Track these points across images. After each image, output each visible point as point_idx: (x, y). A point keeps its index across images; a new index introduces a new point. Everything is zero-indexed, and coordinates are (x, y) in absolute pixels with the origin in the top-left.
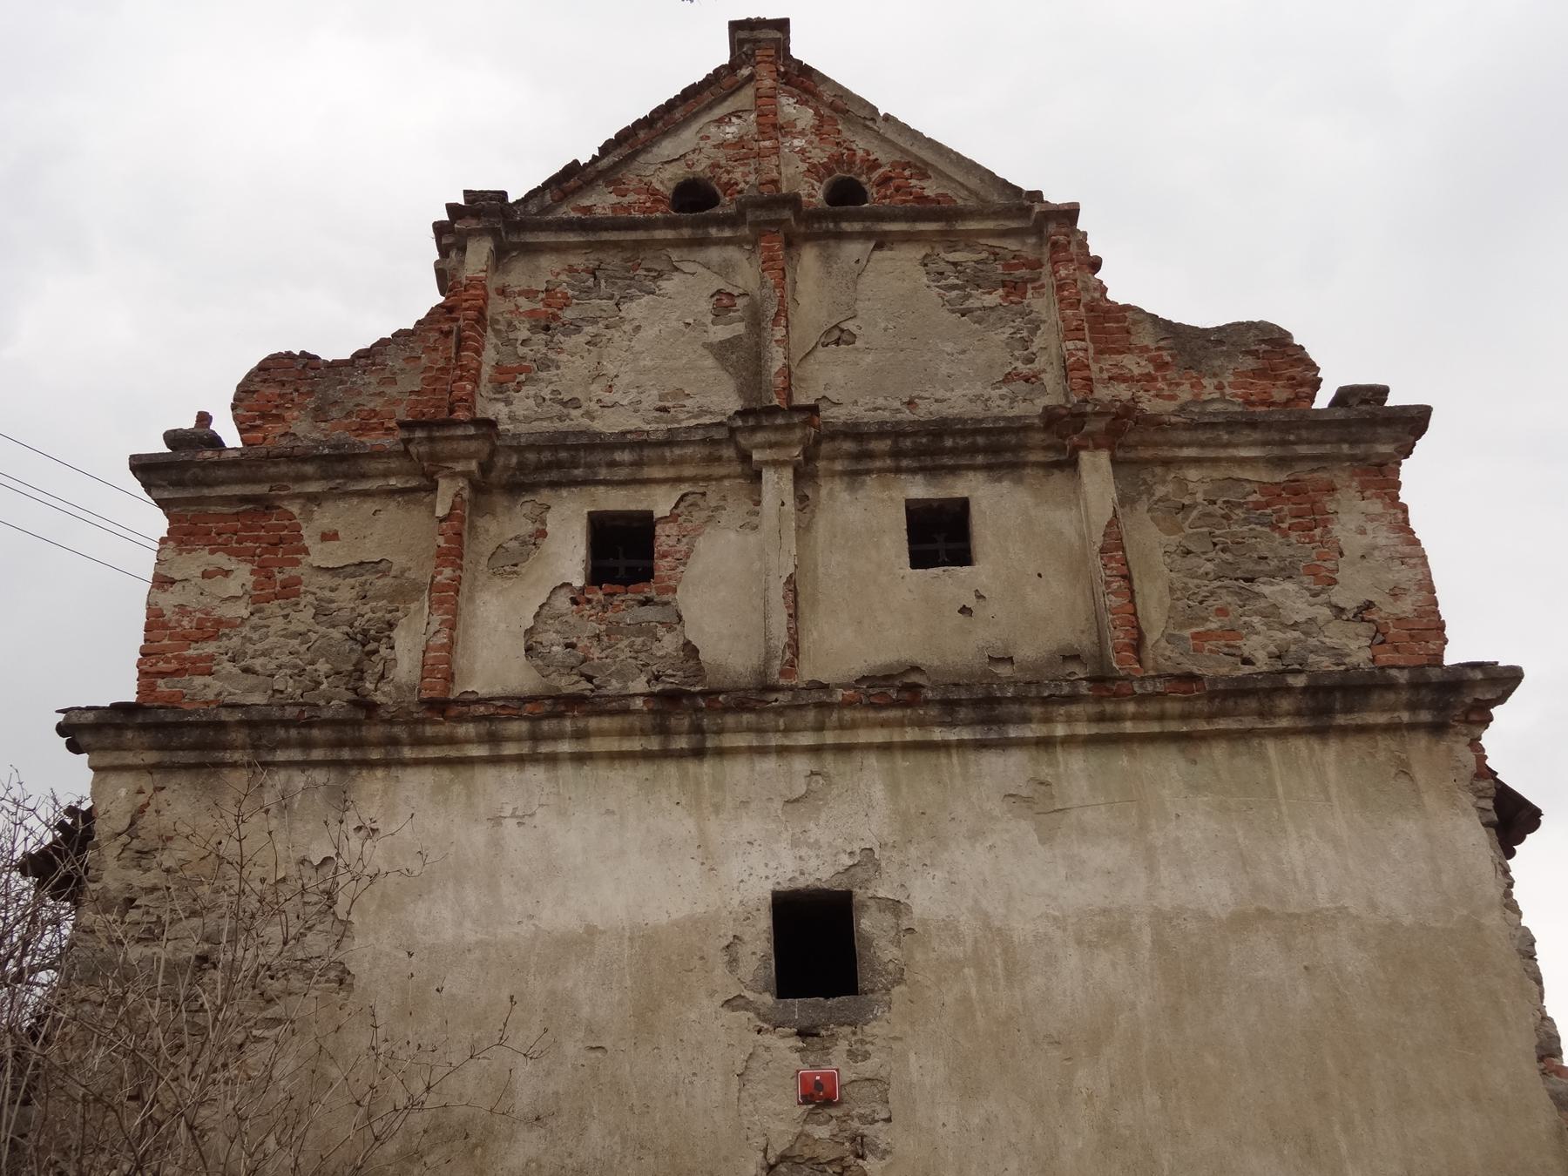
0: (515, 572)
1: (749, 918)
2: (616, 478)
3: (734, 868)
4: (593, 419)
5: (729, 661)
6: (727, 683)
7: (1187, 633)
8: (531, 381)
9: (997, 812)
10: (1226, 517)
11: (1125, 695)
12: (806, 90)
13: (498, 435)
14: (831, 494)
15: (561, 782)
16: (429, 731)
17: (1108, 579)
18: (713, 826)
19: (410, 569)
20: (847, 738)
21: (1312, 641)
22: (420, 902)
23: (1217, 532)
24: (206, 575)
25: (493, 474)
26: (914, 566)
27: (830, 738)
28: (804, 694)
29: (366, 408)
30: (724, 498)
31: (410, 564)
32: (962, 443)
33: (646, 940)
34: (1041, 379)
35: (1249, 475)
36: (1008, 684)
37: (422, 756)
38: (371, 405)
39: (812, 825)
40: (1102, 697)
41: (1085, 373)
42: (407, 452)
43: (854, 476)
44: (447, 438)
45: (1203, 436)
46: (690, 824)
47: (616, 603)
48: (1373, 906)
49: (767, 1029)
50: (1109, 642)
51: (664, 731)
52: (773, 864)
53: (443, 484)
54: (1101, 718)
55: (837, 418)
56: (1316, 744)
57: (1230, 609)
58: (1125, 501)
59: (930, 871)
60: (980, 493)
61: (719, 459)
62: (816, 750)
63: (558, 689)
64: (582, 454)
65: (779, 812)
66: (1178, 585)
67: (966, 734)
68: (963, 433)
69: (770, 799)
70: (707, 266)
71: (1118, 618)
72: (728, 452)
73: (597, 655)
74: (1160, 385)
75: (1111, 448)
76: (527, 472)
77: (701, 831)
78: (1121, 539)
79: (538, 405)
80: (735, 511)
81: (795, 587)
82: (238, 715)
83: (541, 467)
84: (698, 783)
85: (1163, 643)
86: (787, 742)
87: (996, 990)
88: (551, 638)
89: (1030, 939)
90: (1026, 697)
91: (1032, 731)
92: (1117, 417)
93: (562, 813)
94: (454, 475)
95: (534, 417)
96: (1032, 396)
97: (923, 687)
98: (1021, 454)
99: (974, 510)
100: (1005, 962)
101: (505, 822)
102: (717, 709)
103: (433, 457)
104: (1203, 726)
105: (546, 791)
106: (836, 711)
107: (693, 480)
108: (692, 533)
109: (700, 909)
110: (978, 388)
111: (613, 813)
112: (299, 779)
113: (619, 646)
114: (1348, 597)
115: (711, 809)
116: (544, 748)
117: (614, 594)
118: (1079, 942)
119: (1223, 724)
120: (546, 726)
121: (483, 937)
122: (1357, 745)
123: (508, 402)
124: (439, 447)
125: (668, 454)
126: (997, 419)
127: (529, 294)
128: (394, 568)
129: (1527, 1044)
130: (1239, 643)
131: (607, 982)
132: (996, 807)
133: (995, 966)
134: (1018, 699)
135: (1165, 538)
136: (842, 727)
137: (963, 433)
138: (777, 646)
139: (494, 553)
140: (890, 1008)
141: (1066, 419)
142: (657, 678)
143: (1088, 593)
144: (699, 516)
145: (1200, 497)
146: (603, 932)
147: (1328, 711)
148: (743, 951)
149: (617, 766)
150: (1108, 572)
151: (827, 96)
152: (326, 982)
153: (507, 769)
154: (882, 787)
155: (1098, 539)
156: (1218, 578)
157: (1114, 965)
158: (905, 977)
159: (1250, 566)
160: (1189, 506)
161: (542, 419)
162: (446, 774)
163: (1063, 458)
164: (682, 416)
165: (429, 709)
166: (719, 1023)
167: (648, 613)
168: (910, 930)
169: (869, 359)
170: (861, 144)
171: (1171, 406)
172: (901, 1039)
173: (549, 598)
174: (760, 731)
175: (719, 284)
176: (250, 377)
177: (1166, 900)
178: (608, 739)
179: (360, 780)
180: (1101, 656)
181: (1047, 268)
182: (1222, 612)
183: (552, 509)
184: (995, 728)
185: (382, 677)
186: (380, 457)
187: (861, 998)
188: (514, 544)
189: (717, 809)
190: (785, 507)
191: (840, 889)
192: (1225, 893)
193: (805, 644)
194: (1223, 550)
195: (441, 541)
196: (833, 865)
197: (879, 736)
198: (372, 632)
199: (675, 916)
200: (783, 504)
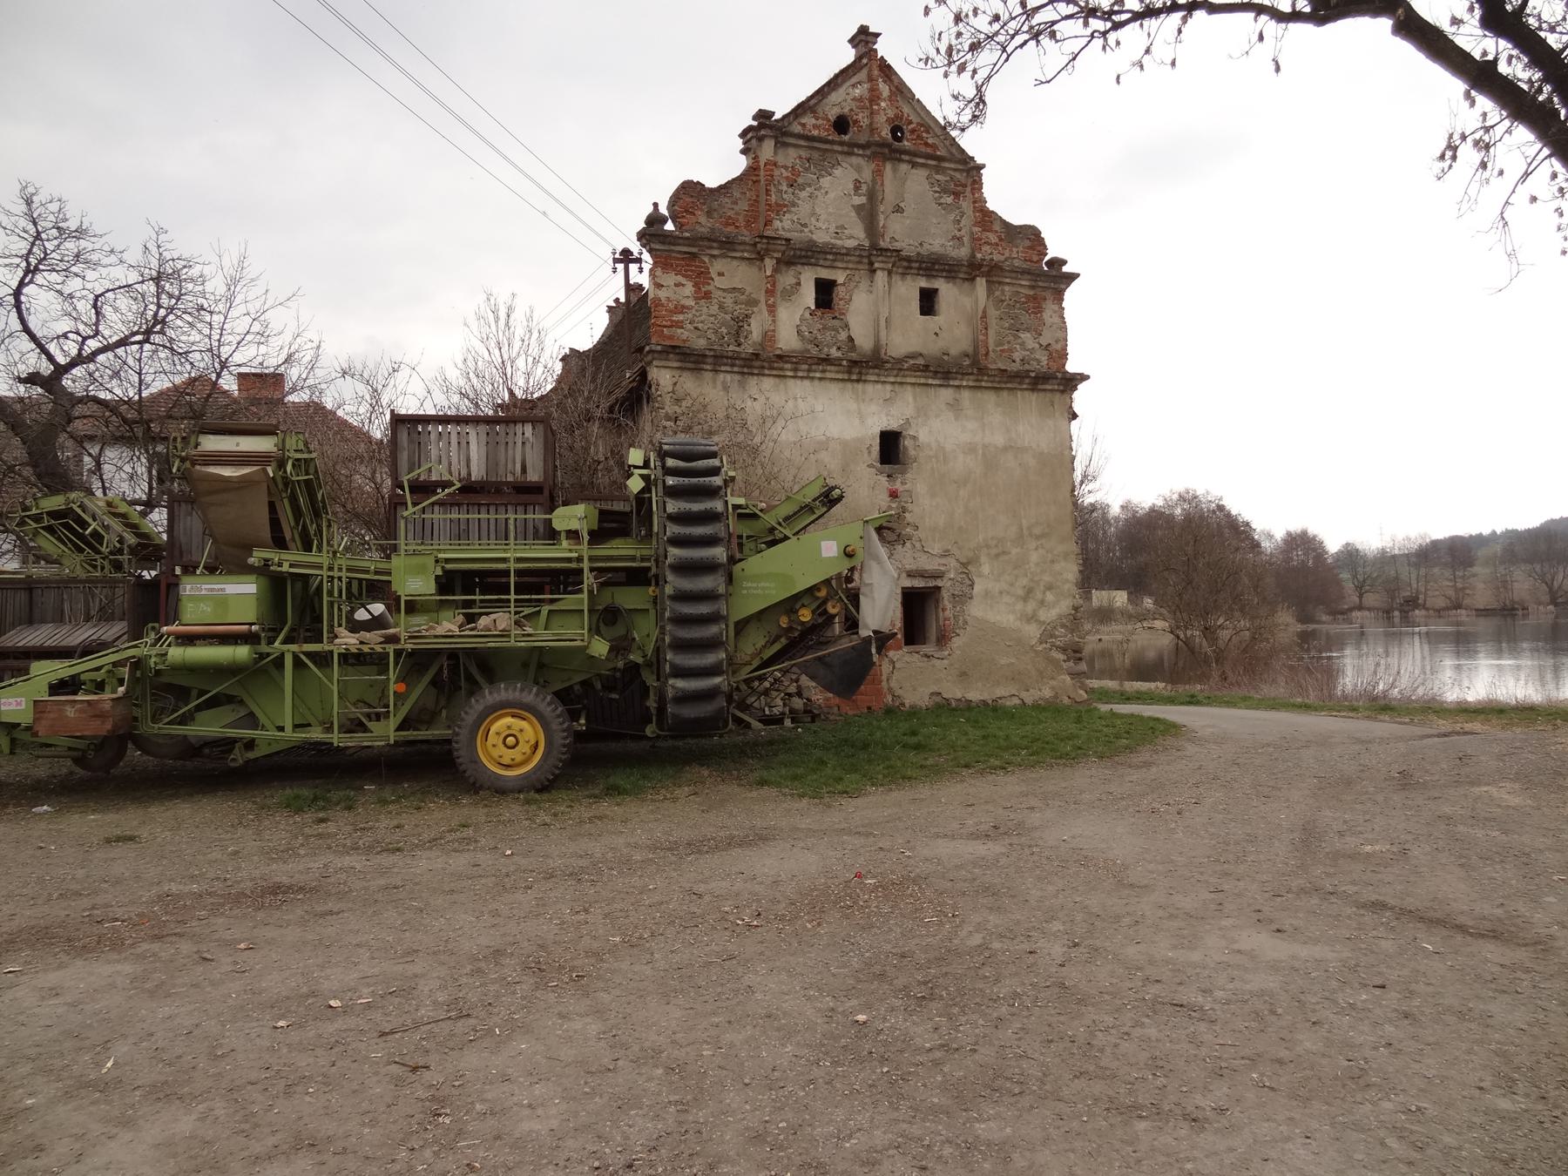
3: (870, 421)
7: (998, 349)
8: (789, 212)
12: (887, 76)
24: (676, 285)
27: (899, 380)
33: (845, 444)
35: (1022, 291)
45: (1014, 275)
48: (1038, 446)
51: (850, 373)
54: (977, 380)
70: (851, 165)
77: (859, 409)
80: (864, 284)
82: (712, 353)
83: (800, 257)
88: (804, 328)
91: (957, 383)
94: (772, 258)
107: (852, 269)
110: (943, 241)
112: (728, 377)
114: (1044, 341)
116: (811, 375)
119: (1009, 385)
120: (814, 367)
122: (1041, 394)
123: (781, 221)
127: (786, 168)
129: (1070, 489)
134: (956, 373)
144: (853, 284)
151: (896, 81)
162: (777, 380)
167: (836, 322)
169: (908, 222)
170: (906, 110)
174: (879, 375)
175: (857, 177)
176: (678, 191)
181: (969, 189)
182: (1009, 342)
197: (913, 380)
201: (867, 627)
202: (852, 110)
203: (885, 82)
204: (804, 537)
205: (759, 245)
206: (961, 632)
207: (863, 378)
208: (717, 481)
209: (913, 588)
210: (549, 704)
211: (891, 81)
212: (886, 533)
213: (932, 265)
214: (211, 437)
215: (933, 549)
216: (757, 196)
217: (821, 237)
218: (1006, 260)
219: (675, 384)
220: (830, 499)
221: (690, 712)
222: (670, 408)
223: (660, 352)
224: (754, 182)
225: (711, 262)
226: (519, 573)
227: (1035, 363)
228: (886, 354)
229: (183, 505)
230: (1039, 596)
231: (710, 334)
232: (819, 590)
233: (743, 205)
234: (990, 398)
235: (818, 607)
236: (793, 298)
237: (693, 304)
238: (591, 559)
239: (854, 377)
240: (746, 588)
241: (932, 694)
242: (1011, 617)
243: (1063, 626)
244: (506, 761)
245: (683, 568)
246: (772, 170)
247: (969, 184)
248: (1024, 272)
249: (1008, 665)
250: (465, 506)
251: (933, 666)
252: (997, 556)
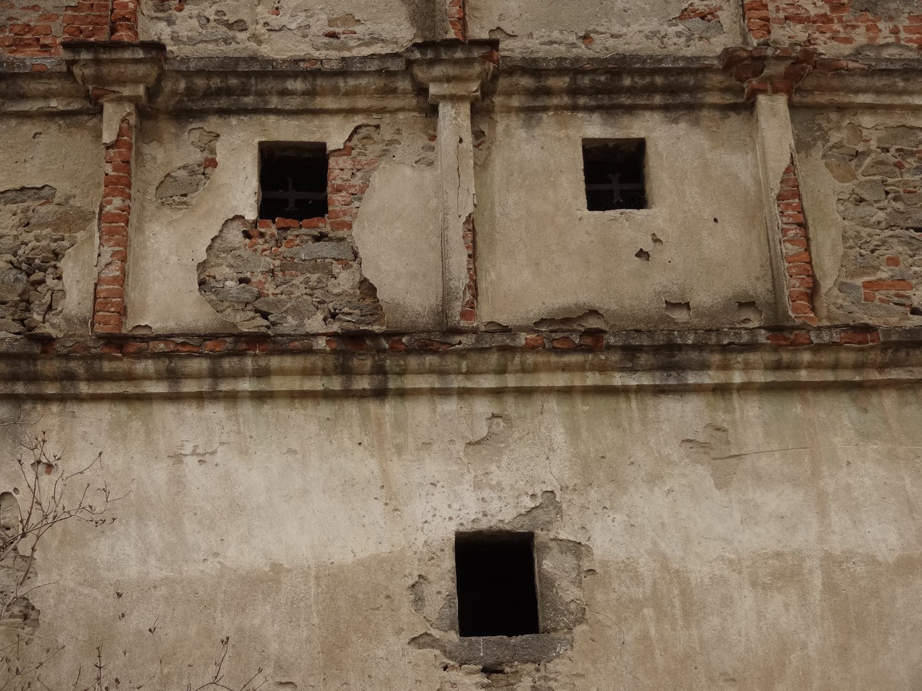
0: (184, 203)
1: (433, 558)
2: (288, 107)
3: (418, 509)
4: (260, 43)
5: (406, 300)
6: (405, 323)
7: (859, 282)
9: (675, 457)
10: (899, 165)
11: (802, 344)
13: (166, 59)
14: (507, 130)
15: (241, 420)
16: (107, 366)
17: (785, 226)
18: (396, 467)
19: (74, 196)
20: (528, 381)
22: (103, 539)
23: (890, 181)
25: (160, 99)
26: (592, 207)
27: (511, 381)
28: (487, 337)
29: (19, 22)
30: (398, 131)
31: (75, 191)
32: (640, 82)
34: (718, 17)
36: (689, 330)
37: (99, 392)
38: (25, 20)
39: (493, 468)
40: (781, 346)
41: (763, 13)
42: (69, 74)
43: (530, 113)
44: (114, 61)
45: (879, 82)
46: (373, 464)
47: (290, 237)
49: (453, 666)
50: (786, 291)
51: (346, 371)
52: (456, 506)
53: (109, 109)
54: (778, 366)
55: (512, 50)
57: (901, 258)
58: (802, 146)
59: (610, 513)
60: (656, 134)
61: (394, 91)
62: (497, 393)
63: (234, 326)
64: (253, 81)
65: (461, 453)
66: (851, 233)
67: (645, 380)
68: (642, 72)
69: (451, 441)
71: (795, 266)
72: (404, 84)
73: (271, 291)
74: (836, 26)
75: (789, 92)
76: (195, 98)
77: (384, 471)
78: (798, 187)
79: (202, 26)
81: (473, 227)
83: (208, 94)
84: (380, 424)
85: (836, 292)
86: (469, 385)
87: (674, 630)
88: (222, 271)
89: (706, 581)
90: (706, 344)
92: (797, 61)
93: (243, 452)
94: (120, 100)
95: (199, 38)
96: (708, 34)
97: (604, 332)
98: (699, 96)
99: (650, 150)
100: (683, 602)
101: (185, 459)
102: (400, 351)
103: (99, 80)
104: (875, 376)
105: (227, 429)
106: (518, 355)
107: (367, 111)
108: (367, 168)
109: (385, 549)
110: (654, 25)
111: (295, 452)
113: (294, 282)
115: (394, 450)
117: (288, 228)
118: (754, 584)
119: (894, 374)
120: (227, 364)
121: (168, 574)
123: (170, 22)
124: (105, 70)
125: (341, 83)
126: (676, 59)
128: (58, 194)
130: (909, 293)
131: (294, 619)
132: (674, 452)
133: (673, 606)
134: (698, 347)
135: (838, 185)
136: (524, 370)
137: (642, 72)
138: (457, 288)
139: (162, 182)
140: (572, 646)
141: (746, 62)
142: (334, 316)
143: (764, 240)
144: (373, 150)
145: (873, 145)
146: (289, 571)
148: (429, 591)
149: (297, 405)
150: (785, 220)
152: (11, 617)
153: (186, 407)
154: (562, 430)
155: (775, 186)
156: (890, 227)
157: (787, 606)
158: (587, 616)
160: (863, 153)
161: (206, 41)
162: (123, 410)
163: (740, 100)
164: (352, 43)
165: (106, 345)
166: (406, 660)
167: (324, 250)
168: (591, 571)
171: (847, 49)
172: (582, 676)
173: (221, 231)
174: (442, 373)
177: (836, 545)
178: (290, 378)
179: (34, 415)
180: (775, 303)
182: (893, 261)
183: (222, 137)
184: (674, 374)
185: (50, 308)
186: (41, 77)
187: (545, 637)
188: (182, 174)
190: (464, 145)
191: (522, 531)
192: (893, 538)
193: (482, 286)
194: (895, 199)
195: (109, 169)
196: (515, 507)
197: (560, 380)
198: (37, 261)
199: (361, 555)
200: (461, 141)
207: (392, 385)
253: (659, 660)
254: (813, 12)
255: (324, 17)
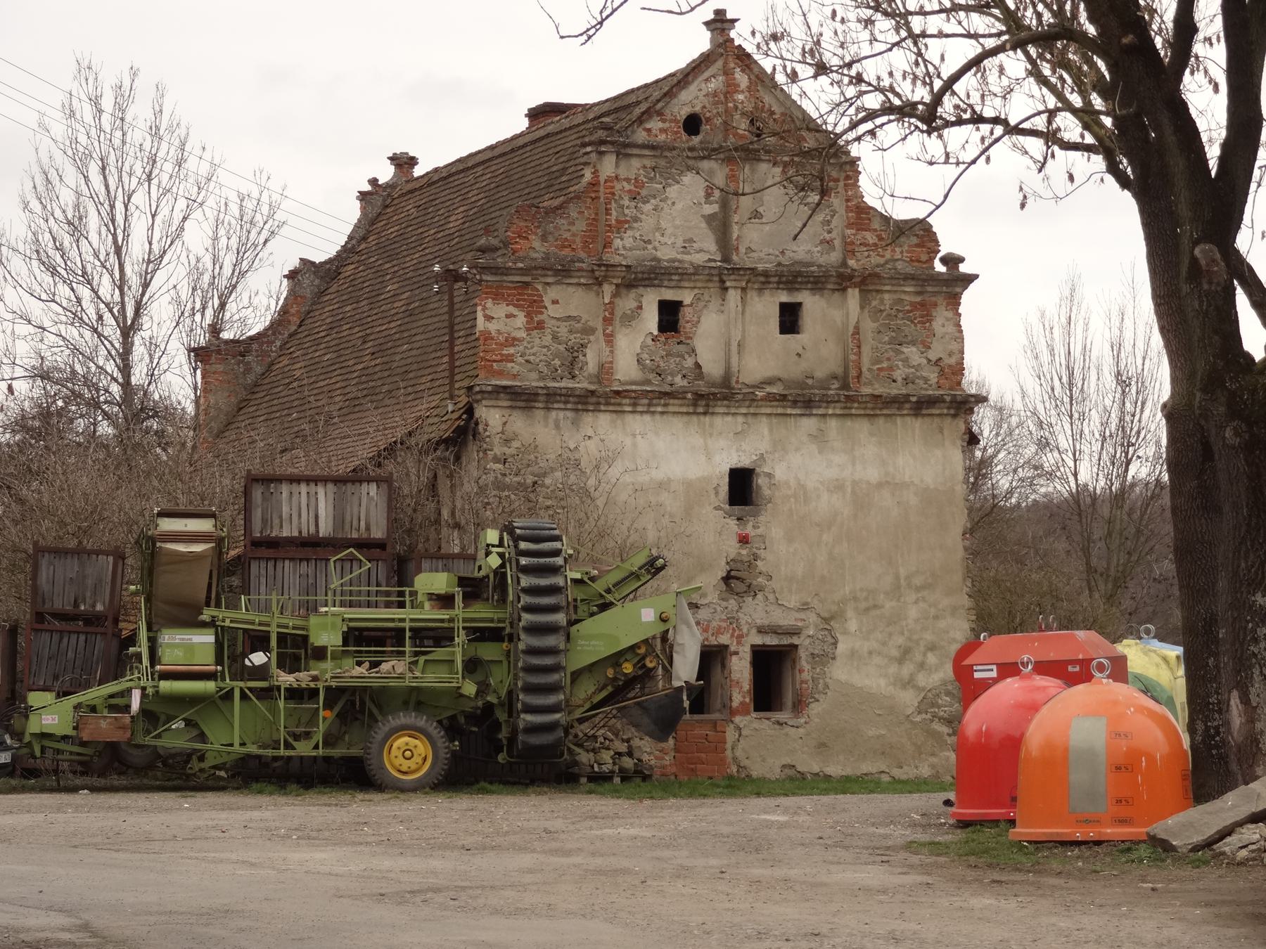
3: (717, 458)
7: (875, 367)
8: (631, 228)
14: (752, 299)
21: (918, 374)
24: (508, 316)
27: (752, 410)
33: (688, 484)
35: (907, 298)
45: (894, 282)
46: (702, 441)
48: (922, 481)
51: (695, 405)
54: (845, 408)
56: (914, 419)
62: (745, 414)
80: (715, 304)
82: (545, 392)
88: (645, 356)
91: (821, 411)
104: (878, 412)
109: (706, 474)
110: (809, 247)
112: (561, 414)
114: (933, 356)
119: (885, 412)
120: (654, 401)
122: (927, 419)
123: (622, 239)
127: (628, 180)
144: (701, 304)
147: (921, 409)
151: (756, 70)
155: (851, 329)
159: (901, 339)
162: (614, 415)
170: (768, 99)
174: (728, 407)
181: (841, 184)
182: (889, 359)
189: (711, 435)
197: (768, 411)
201: (679, 679)
202: (704, 107)
203: (743, 71)
204: (628, 605)
205: (597, 273)
206: (821, 697)
208: (559, 561)
209: (764, 645)
210: (436, 728)
211: (751, 70)
212: (733, 583)
213: (792, 277)
214: (166, 519)
215: (789, 602)
216: (597, 214)
217: (666, 254)
218: (887, 262)
219: (505, 424)
220: (654, 567)
221: (535, 740)
222: (498, 450)
223: (489, 392)
224: (593, 199)
225: (545, 290)
226: (411, 629)
227: (921, 382)
228: (737, 382)
229: (47, 555)
230: (918, 657)
231: (542, 367)
232: (639, 648)
233: (581, 226)
234: (862, 428)
235: (639, 662)
236: (633, 323)
237: (524, 335)
238: (465, 620)
239: (701, 410)
240: (581, 645)
241: (784, 766)
242: (882, 682)
243: (948, 693)
244: (404, 769)
245: (534, 630)
246: (613, 187)
247: (842, 178)
248: (908, 278)
249: (878, 737)
250: (314, 562)
251: (787, 735)
252: (867, 610)
253: (795, 517)
254: (871, 242)
255: (681, 239)
